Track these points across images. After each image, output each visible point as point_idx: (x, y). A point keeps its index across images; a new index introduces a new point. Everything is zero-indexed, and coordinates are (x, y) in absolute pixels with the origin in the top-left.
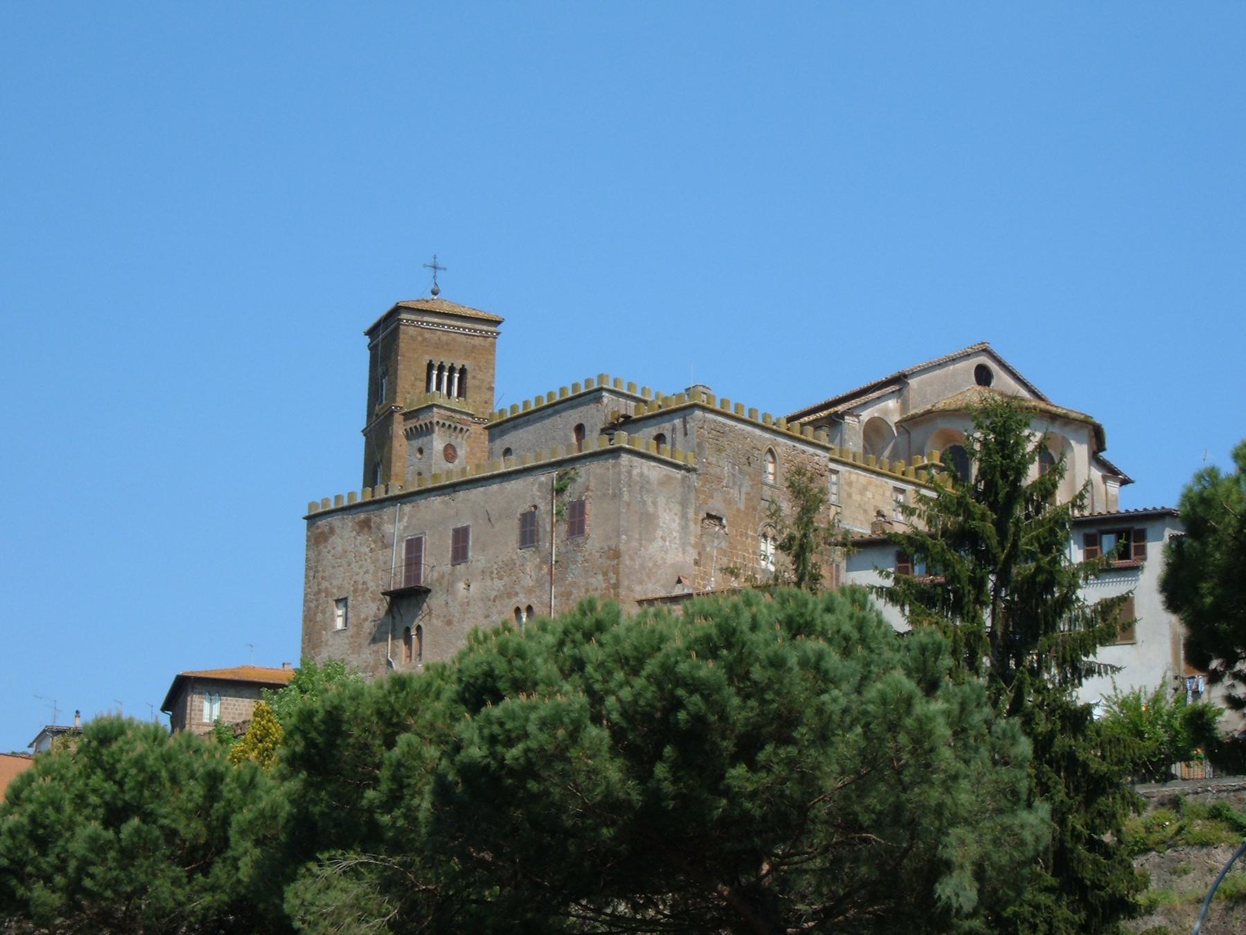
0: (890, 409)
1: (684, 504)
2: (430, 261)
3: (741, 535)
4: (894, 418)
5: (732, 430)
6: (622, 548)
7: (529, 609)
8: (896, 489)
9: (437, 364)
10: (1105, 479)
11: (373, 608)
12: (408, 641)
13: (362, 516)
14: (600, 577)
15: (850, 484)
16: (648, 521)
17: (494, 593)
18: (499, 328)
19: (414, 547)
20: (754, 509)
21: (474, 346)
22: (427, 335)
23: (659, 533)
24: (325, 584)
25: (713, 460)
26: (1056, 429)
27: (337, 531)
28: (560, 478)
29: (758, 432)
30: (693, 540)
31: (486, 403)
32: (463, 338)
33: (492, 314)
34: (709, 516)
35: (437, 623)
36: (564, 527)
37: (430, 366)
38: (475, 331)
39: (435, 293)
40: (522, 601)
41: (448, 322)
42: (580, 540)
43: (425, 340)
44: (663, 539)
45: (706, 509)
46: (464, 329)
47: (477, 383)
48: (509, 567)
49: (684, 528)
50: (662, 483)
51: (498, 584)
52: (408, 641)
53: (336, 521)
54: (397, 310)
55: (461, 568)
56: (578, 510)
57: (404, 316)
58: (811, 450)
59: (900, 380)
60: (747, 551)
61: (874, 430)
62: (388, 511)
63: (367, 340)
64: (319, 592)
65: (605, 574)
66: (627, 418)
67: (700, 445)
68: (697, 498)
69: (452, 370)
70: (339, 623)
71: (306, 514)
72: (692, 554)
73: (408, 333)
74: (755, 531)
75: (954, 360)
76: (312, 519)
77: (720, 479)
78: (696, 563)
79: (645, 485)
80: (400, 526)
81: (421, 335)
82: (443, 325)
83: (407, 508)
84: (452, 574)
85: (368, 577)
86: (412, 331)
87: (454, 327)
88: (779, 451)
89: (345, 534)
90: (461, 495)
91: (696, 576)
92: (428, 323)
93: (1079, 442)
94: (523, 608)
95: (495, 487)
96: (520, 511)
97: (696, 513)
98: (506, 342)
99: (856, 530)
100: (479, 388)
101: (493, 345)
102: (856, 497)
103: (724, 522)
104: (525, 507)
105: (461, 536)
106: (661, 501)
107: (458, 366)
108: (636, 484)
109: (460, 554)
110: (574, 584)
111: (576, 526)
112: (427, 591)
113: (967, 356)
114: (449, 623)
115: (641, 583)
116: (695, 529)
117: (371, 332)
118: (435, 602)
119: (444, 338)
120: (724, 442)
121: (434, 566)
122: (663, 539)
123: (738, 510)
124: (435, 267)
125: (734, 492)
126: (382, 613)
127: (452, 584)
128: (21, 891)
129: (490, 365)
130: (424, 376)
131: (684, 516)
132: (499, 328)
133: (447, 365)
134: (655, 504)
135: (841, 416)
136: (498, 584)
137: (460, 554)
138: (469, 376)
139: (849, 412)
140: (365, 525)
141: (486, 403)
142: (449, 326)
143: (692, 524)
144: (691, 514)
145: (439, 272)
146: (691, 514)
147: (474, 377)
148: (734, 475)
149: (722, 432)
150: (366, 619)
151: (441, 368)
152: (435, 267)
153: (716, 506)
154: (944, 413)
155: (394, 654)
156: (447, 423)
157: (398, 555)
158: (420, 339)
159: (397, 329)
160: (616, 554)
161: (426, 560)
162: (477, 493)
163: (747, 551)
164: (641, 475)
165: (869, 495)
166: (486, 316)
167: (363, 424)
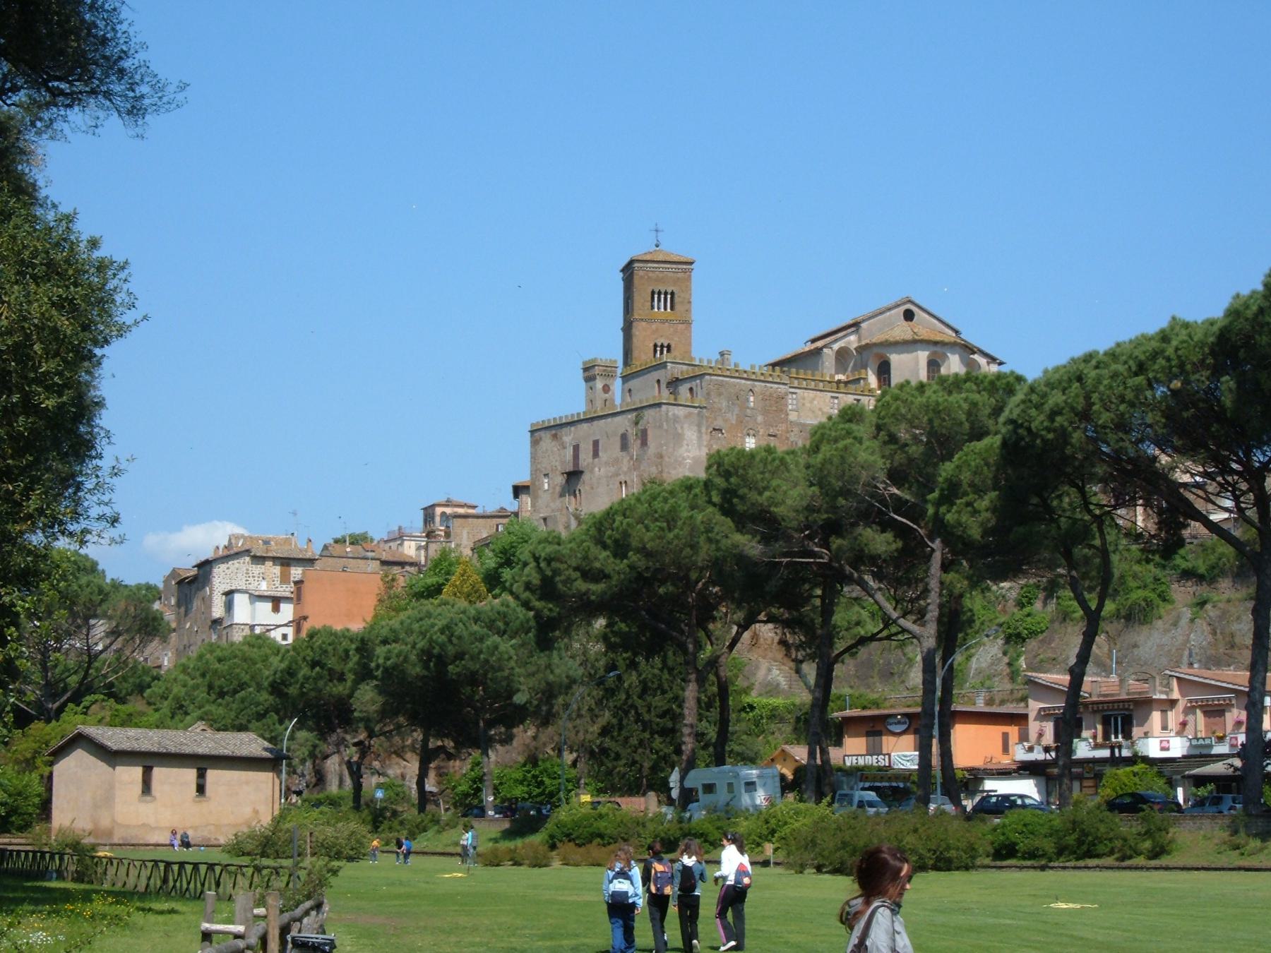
0: (852, 341)
1: (699, 426)
2: (660, 228)
4: (853, 346)
5: (727, 382)
6: (664, 453)
8: (832, 397)
9: (657, 291)
10: (988, 363)
11: (560, 480)
12: (575, 496)
13: (554, 432)
15: (804, 399)
16: (678, 438)
19: (576, 448)
22: (650, 274)
23: (685, 442)
25: (716, 400)
26: (938, 349)
28: (636, 417)
29: (743, 381)
30: (705, 443)
32: (671, 274)
33: (689, 258)
34: (714, 429)
35: (587, 488)
36: (639, 442)
37: (653, 293)
39: (657, 246)
40: (622, 478)
41: (662, 265)
43: (649, 277)
47: (680, 300)
48: (617, 461)
49: (700, 438)
50: (686, 417)
51: (612, 469)
52: (575, 496)
53: (542, 434)
54: (631, 262)
55: (596, 460)
57: (636, 265)
58: (776, 386)
59: (856, 325)
61: (842, 355)
62: (565, 430)
63: (621, 275)
66: (677, 379)
67: (708, 394)
69: (666, 294)
70: (546, 486)
73: (638, 274)
75: (889, 309)
76: (532, 432)
77: (721, 410)
79: (676, 419)
80: (570, 438)
83: (573, 428)
85: (557, 464)
86: (641, 273)
88: (756, 390)
89: (547, 442)
90: (595, 423)
93: (953, 353)
95: (609, 420)
98: (698, 275)
99: (809, 422)
101: (690, 276)
102: (808, 405)
104: (622, 431)
106: (686, 426)
107: (669, 291)
109: (596, 454)
111: (644, 443)
112: (582, 472)
113: (897, 306)
114: (592, 488)
115: (675, 468)
116: (706, 437)
117: (623, 271)
118: (586, 477)
119: (661, 275)
120: (722, 390)
121: (585, 458)
124: (657, 231)
125: (729, 415)
126: (564, 482)
128: (286, 690)
129: (688, 289)
131: (700, 431)
132: (692, 267)
133: (663, 291)
134: (682, 428)
135: (821, 349)
136: (612, 469)
137: (596, 454)
138: (676, 296)
139: (825, 346)
144: (704, 430)
145: (659, 234)
146: (704, 430)
149: (721, 385)
151: (659, 293)
152: (657, 231)
153: (719, 423)
154: (875, 345)
155: (569, 503)
157: (569, 452)
159: (632, 273)
160: (661, 456)
161: (582, 456)
164: (674, 414)
165: (815, 402)
166: (685, 260)
167: (622, 325)
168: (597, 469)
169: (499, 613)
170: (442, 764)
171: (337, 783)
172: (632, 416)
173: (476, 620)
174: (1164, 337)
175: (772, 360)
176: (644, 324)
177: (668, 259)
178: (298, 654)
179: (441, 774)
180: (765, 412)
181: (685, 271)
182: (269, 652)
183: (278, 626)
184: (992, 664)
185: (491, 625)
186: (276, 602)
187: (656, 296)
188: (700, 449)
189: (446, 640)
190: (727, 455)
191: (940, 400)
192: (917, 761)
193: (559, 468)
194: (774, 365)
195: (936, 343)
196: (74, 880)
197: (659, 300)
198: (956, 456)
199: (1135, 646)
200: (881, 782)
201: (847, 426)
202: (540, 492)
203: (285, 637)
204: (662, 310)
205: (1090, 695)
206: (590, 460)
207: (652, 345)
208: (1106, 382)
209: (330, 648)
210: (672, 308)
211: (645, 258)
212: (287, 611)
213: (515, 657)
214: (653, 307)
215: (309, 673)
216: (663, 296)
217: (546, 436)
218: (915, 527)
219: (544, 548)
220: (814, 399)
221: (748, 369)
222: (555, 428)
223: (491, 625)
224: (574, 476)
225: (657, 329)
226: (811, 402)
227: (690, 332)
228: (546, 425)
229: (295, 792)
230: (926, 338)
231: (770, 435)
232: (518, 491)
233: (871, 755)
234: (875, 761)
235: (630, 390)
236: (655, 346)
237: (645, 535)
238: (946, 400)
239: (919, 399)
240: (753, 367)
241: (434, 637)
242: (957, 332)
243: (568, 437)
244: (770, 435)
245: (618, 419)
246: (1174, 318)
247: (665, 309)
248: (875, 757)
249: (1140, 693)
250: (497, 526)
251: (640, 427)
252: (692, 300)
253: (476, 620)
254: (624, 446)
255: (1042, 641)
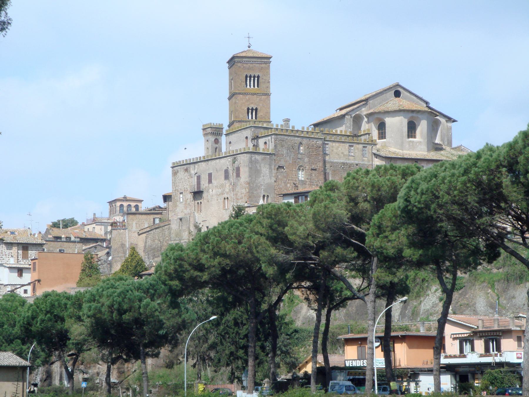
1: (270, 165)
3: (291, 171)
7: (227, 198)
9: (249, 75)
14: (244, 190)
17: (219, 193)
18: (271, 60)
19: (199, 178)
20: (295, 162)
21: (262, 67)
22: (245, 65)
24: (177, 188)
26: (414, 115)
27: (179, 171)
30: (274, 175)
31: (267, 87)
32: (258, 65)
33: (267, 53)
36: (235, 174)
37: (246, 77)
38: (262, 62)
42: (239, 178)
43: (244, 67)
44: (263, 176)
45: (278, 165)
46: (256, 62)
47: (264, 81)
48: (222, 186)
49: (271, 172)
51: (220, 190)
55: (211, 185)
56: (238, 169)
60: (293, 175)
63: (227, 65)
64: (175, 190)
65: (245, 189)
68: (275, 162)
71: (171, 166)
72: (274, 179)
74: (296, 169)
78: (275, 182)
81: (243, 65)
82: (250, 61)
84: (208, 187)
85: (188, 186)
87: (254, 61)
89: (182, 174)
90: (210, 162)
91: (275, 186)
92: (245, 61)
94: (226, 198)
96: (224, 169)
97: (275, 166)
100: (265, 82)
101: (269, 66)
102: (335, 151)
103: (285, 168)
104: (225, 168)
105: (210, 175)
106: (262, 165)
107: (256, 75)
108: (254, 161)
109: (210, 181)
110: (238, 191)
111: (238, 175)
112: (202, 192)
114: (208, 201)
115: (256, 190)
116: (274, 172)
117: (228, 62)
118: (205, 195)
121: (204, 183)
122: (263, 176)
123: (290, 163)
127: (208, 190)
129: (268, 74)
130: (244, 80)
131: (270, 168)
134: (260, 166)
136: (220, 190)
137: (210, 181)
140: (186, 170)
141: (267, 87)
142: (252, 61)
143: (273, 170)
144: (273, 167)
146: (273, 167)
147: (263, 79)
148: (288, 153)
150: (188, 199)
151: (250, 77)
152: (249, 38)
153: (282, 163)
156: (215, 132)
158: (242, 67)
162: (214, 162)
163: (293, 175)
165: (340, 149)
168: (211, 190)
169: (151, 284)
170: (120, 366)
171: (59, 378)
172: (230, 159)
173: (138, 289)
174: (478, 156)
175: (315, 122)
176: (241, 96)
177: (256, 55)
178: (38, 307)
179: (121, 373)
180: (310, 156)
181: (266, 63)
182: (18, 304)
183: (23, 285)
184: (433, 307)
185: (146, 291)
186: (20, 271)
187: (248, 78)
188: (271, 179)
189: (121, 300)
190: (266, 208)
191: (375, 180)
192: (384, 364)
193: (189, 190)
194: (316, 125)
195: (413, 111)
196: (188, 384)
197: (250, 81)
198: (380, 211)
199: (514, 297)
200: (359, 376)
201: (328, 193)
202: (178, 203)
203: (26, 291)
204: (252, 87)
205: (478, 327)
206: (207, 185)
207: (246, 109)
208: (448, 179)
209: (56, 303)
210: (258, 86)
211: (241, 55)
212: (27, 278)
213: (159, 310)
214: (247, 86)
215: (44, 317)
216: (252, 79)
217: (180, 169)
218: (362, 245)
219: (174, 253)
220: (338, 147)
221: (300, 129)
222: (186, 165)
223: (146, 291)
224: (198, 194)
225: (249, 99)
226: (337, 149)
227: (270, 101)
228: (181, 163)
229: (33, 384)
230: (407, 109)
231: (312, 169)
232: (166, 198)
233: (360, 360)
234: (351, 363)
235: (230, 143)
236: (248, 109)
237: (228, 247)
238: (378, 181)
239: (365, 179)
240: (303, 128)
241: (115, 299)
242: (427, 103)
243: (193, 170)
244: (312, 169)
245: (223, 161)
246: (487, 144)
247: (254, 86)
248: (362, 361)
249: (505, 327)
250: (154, 219)
251: (236, 164)
252: (271, 81)
253: (138, 289)
254: (227, 177)
255: (461, 294)
